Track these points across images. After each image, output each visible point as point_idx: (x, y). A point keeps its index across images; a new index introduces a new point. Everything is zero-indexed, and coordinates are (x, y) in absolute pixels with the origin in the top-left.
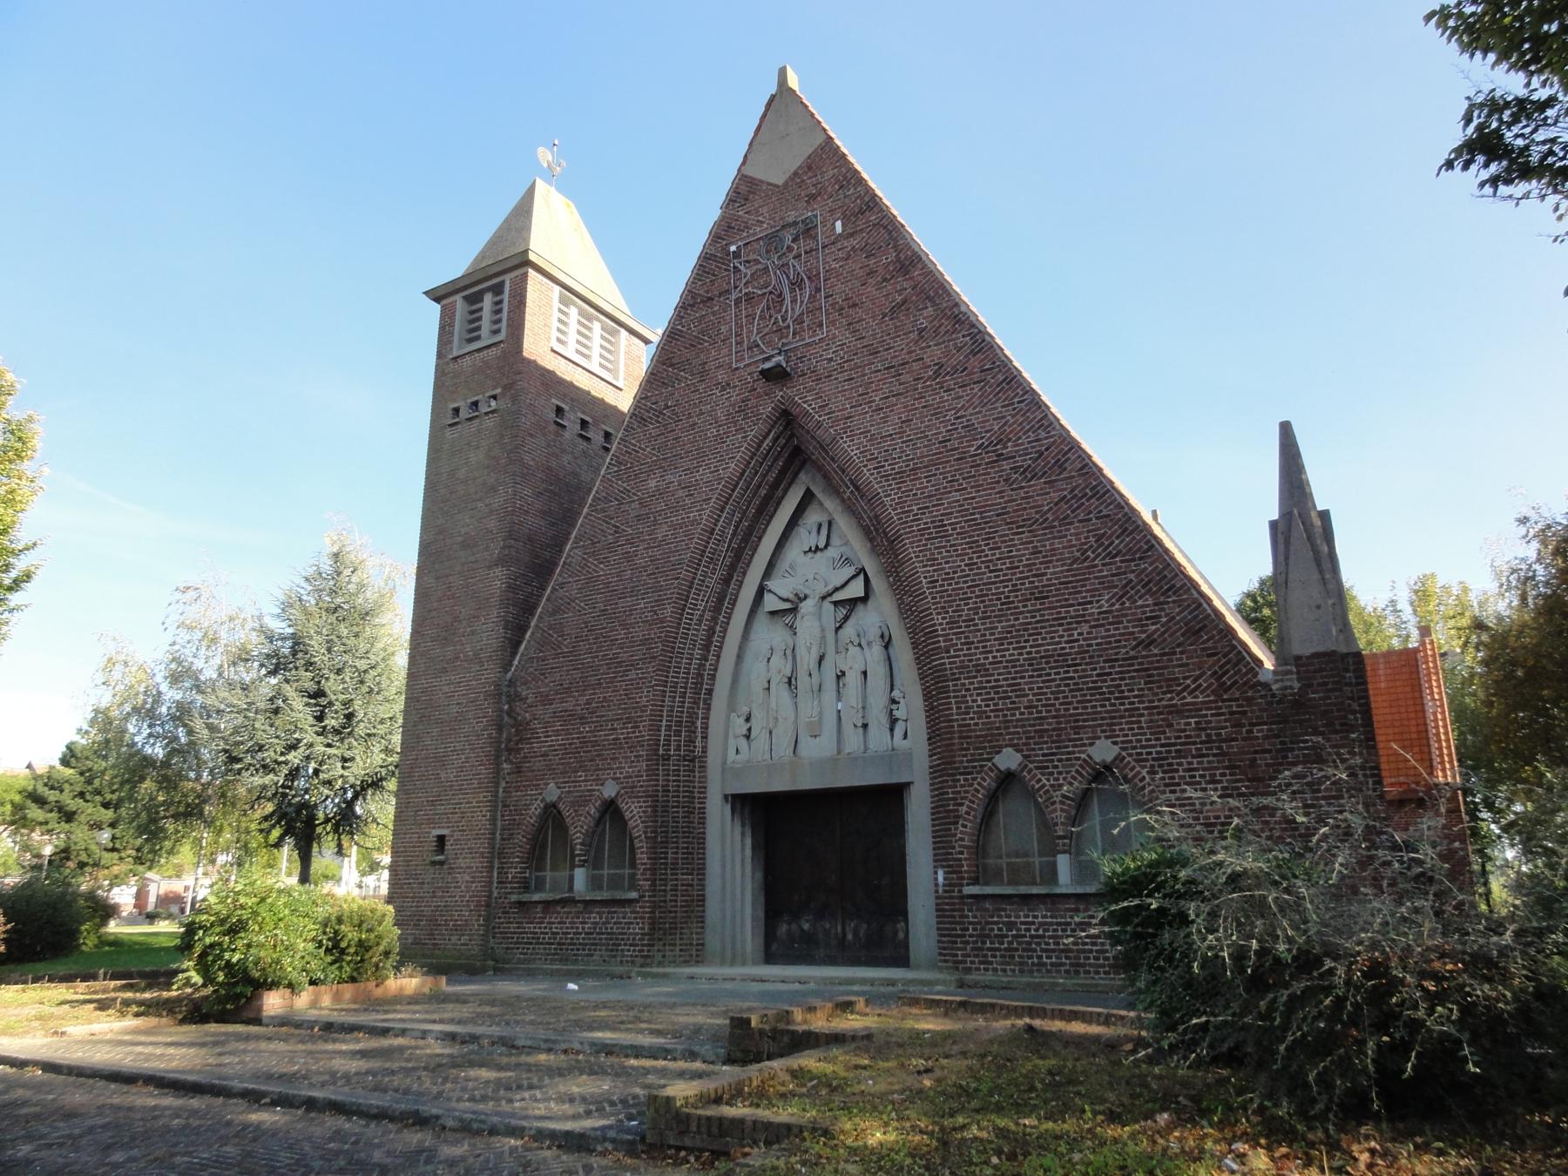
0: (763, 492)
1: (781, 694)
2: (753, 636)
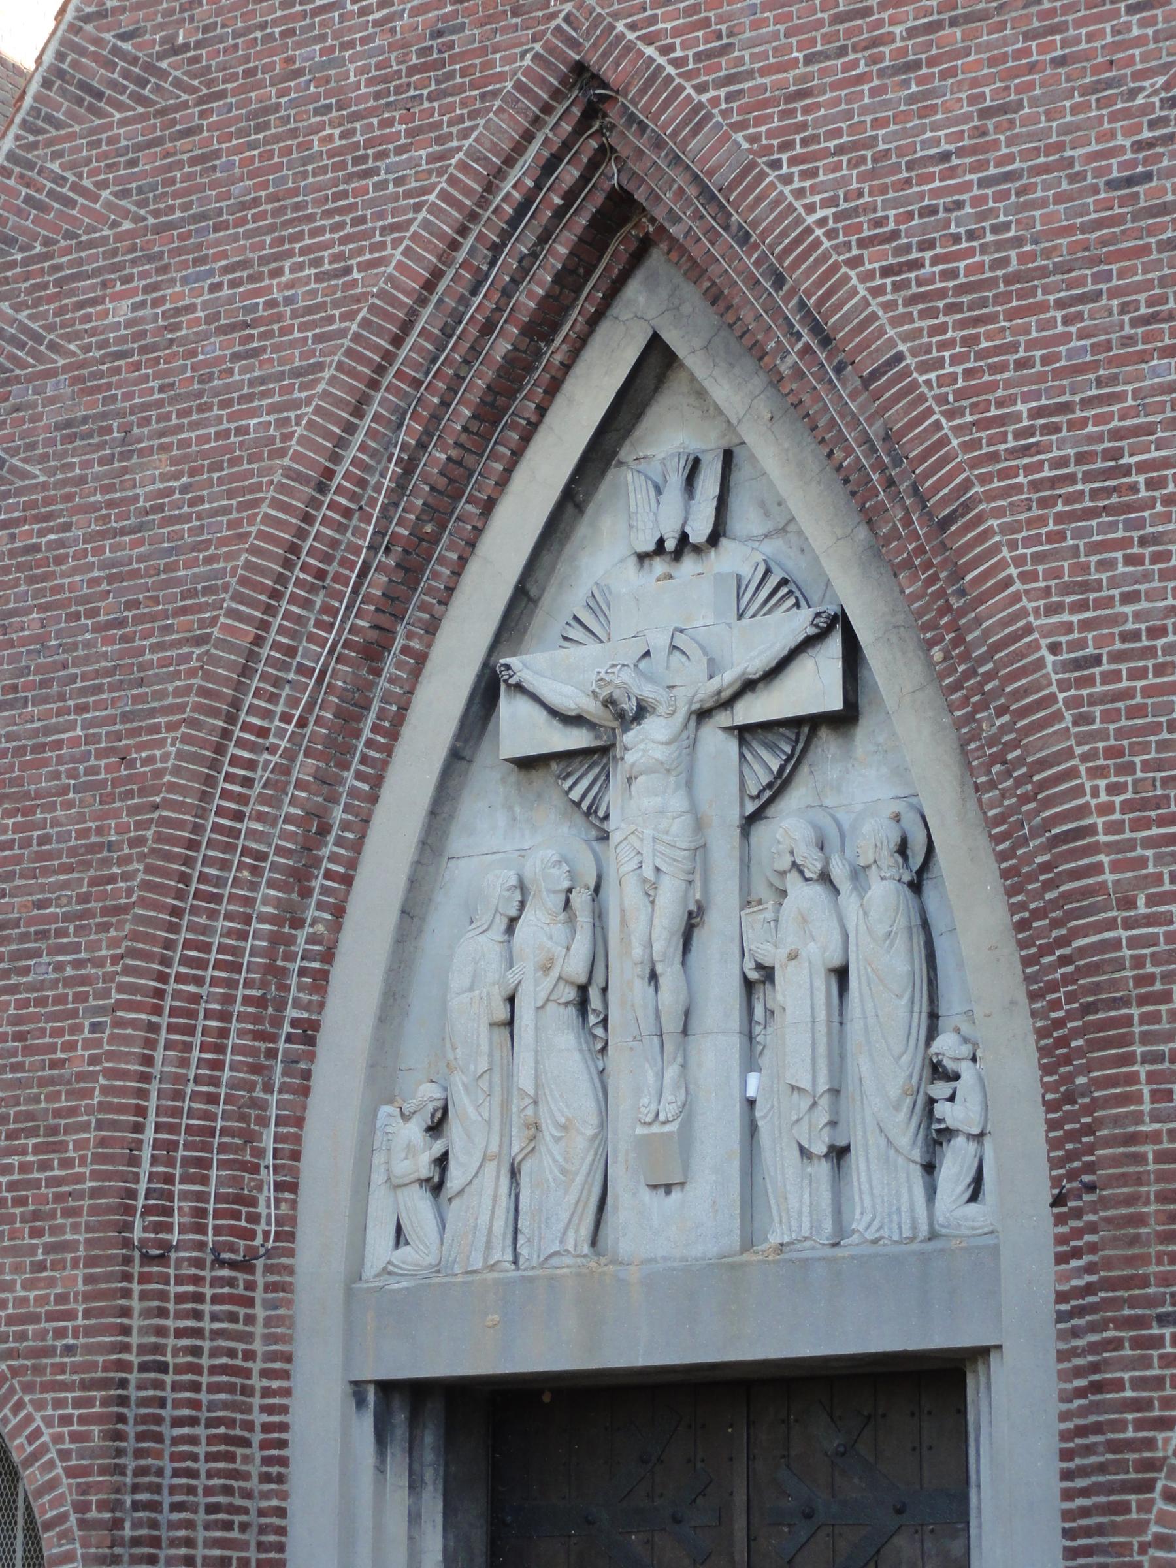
0: (500, 348)
1: (552, 1045)
2: (457, 843)
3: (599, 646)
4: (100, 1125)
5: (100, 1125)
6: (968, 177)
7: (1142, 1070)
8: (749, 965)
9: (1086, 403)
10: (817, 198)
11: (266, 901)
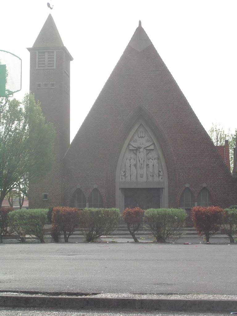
1: (133, 168)
11: (15, 233)
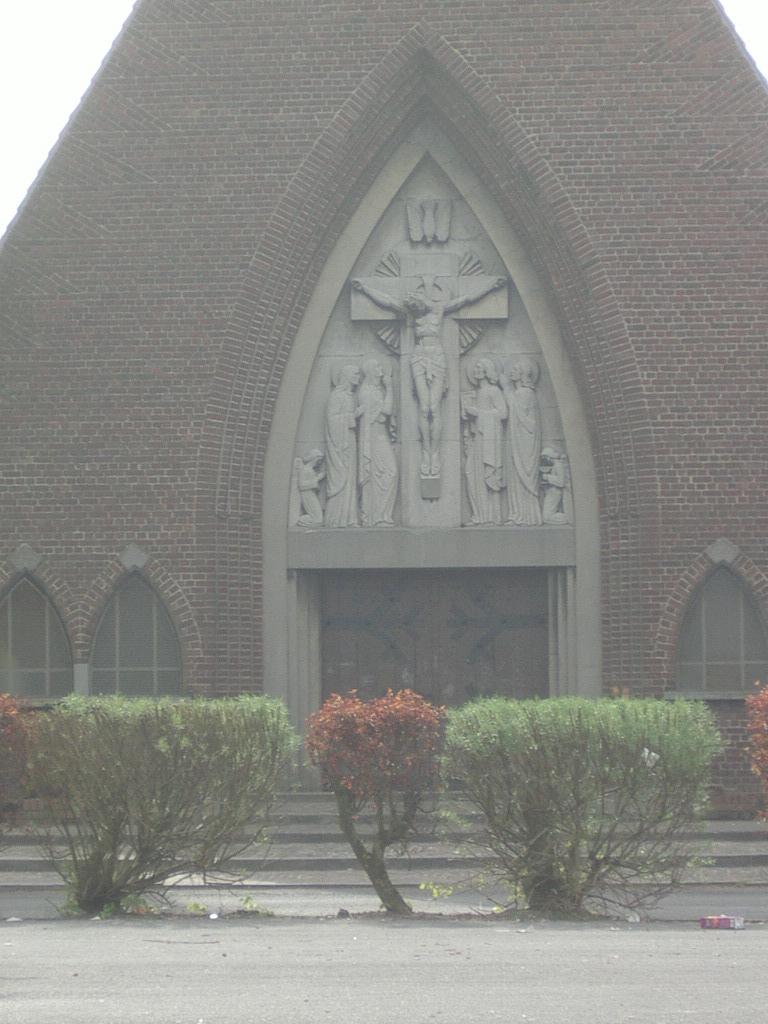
1: (375, 442)
3: (395, 278)
4: (202, 465)
5: (202, 465)
6: (596, 133)
7: (658, 477)
8: (464, 414)
9: (642, 230)
10: (532, 128)
